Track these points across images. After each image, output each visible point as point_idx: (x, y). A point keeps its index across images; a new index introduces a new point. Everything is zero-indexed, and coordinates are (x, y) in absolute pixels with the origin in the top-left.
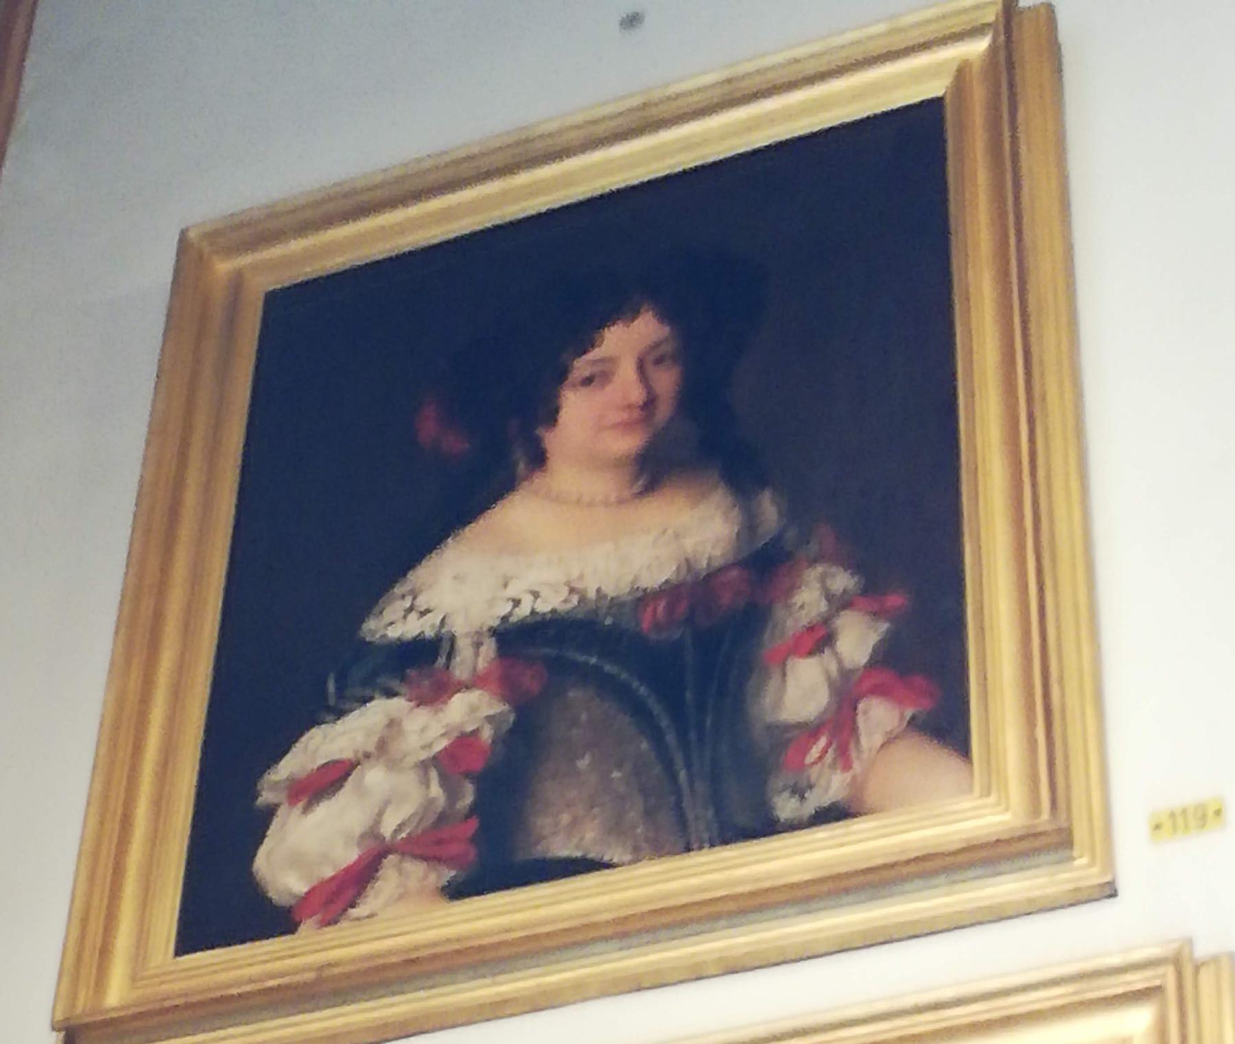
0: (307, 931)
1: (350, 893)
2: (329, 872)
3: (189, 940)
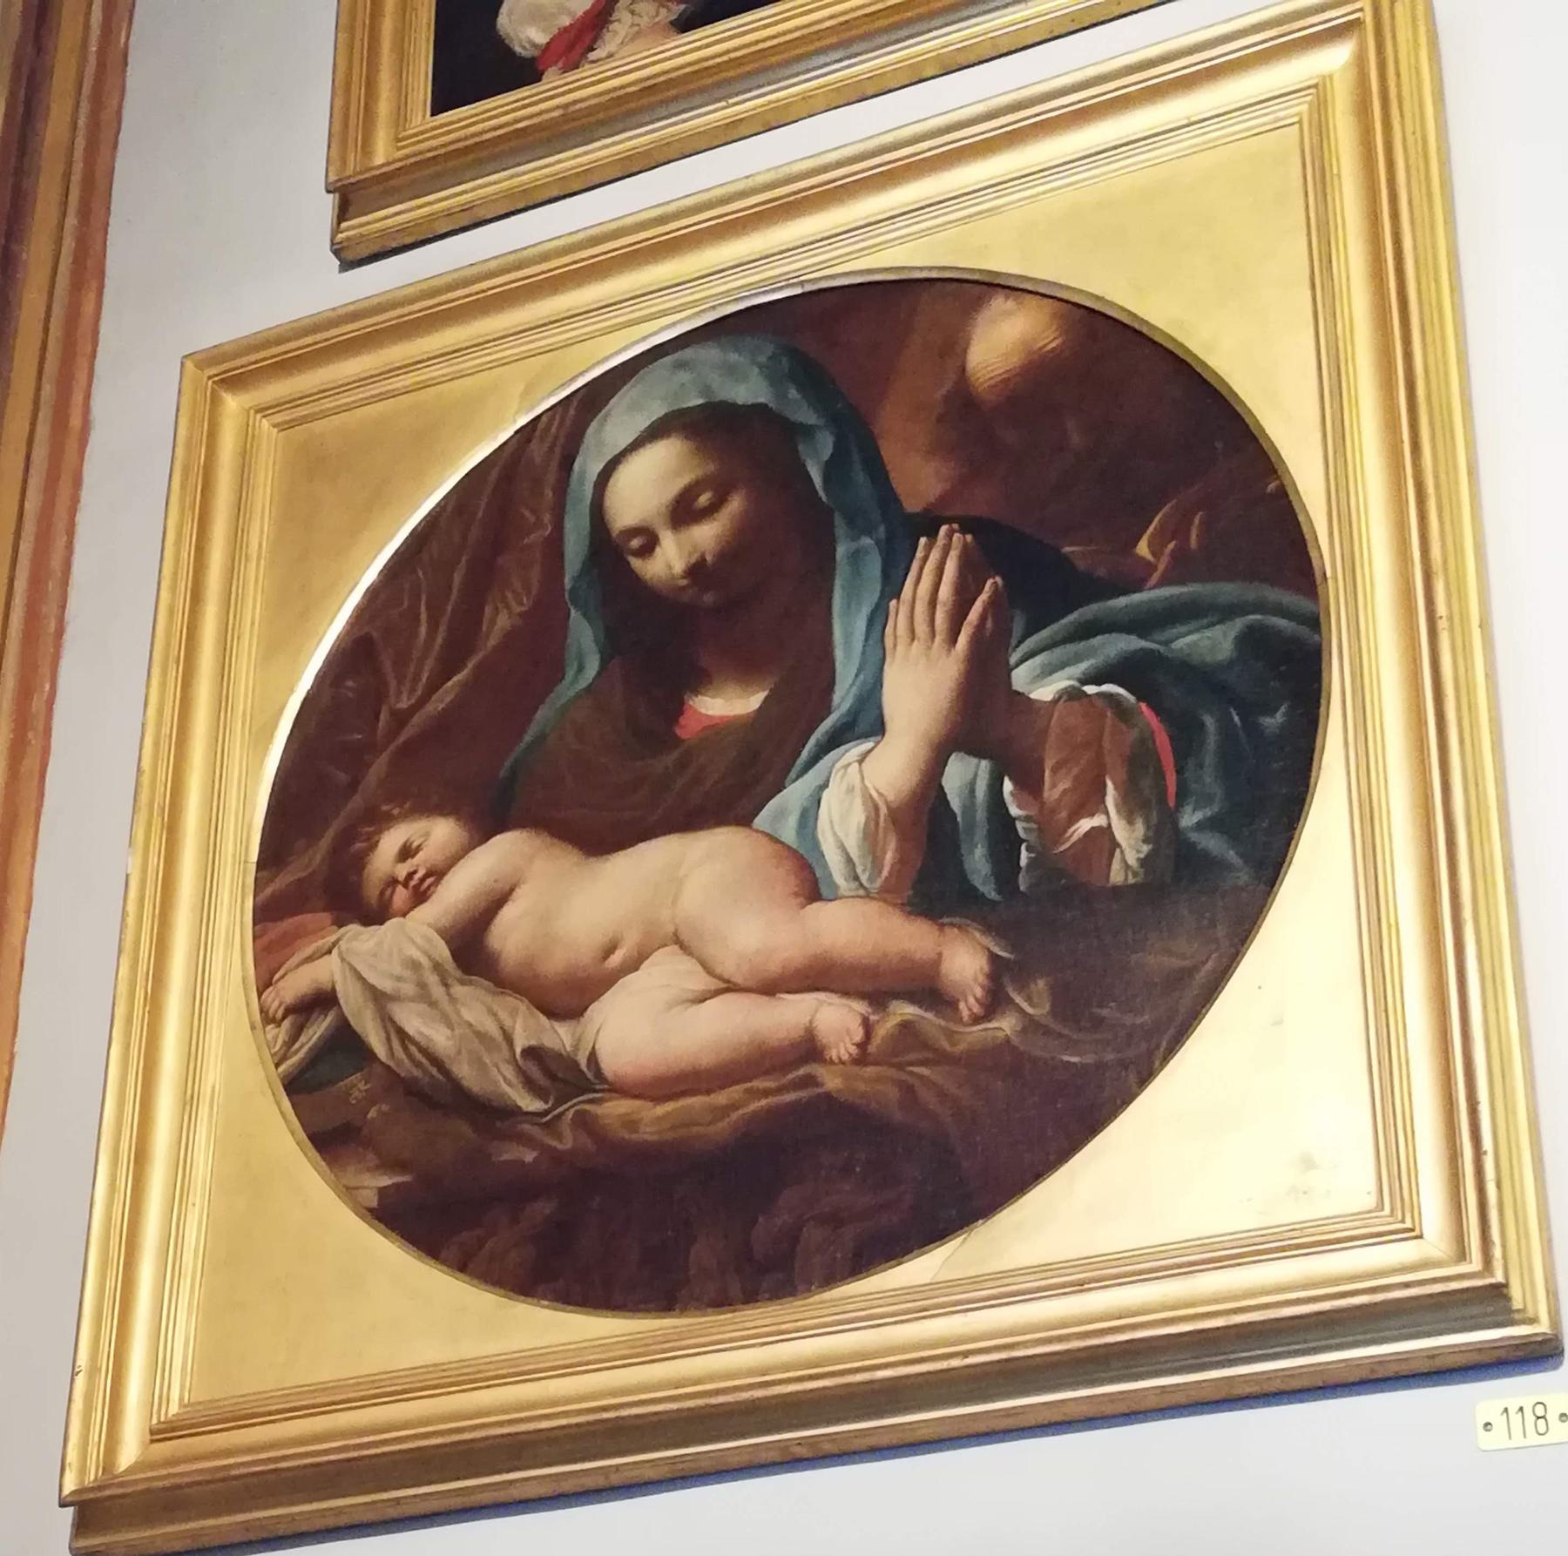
0: (552, 80)
1: (587, 39)
2: (566, 21)
3: (441, 104)
